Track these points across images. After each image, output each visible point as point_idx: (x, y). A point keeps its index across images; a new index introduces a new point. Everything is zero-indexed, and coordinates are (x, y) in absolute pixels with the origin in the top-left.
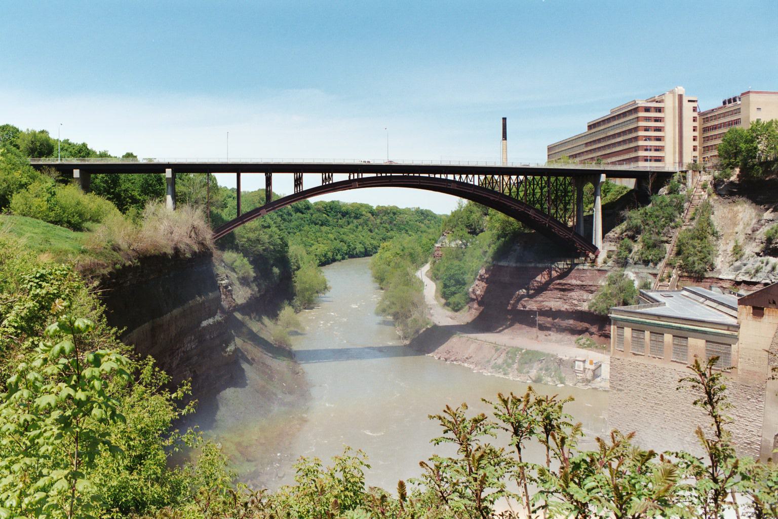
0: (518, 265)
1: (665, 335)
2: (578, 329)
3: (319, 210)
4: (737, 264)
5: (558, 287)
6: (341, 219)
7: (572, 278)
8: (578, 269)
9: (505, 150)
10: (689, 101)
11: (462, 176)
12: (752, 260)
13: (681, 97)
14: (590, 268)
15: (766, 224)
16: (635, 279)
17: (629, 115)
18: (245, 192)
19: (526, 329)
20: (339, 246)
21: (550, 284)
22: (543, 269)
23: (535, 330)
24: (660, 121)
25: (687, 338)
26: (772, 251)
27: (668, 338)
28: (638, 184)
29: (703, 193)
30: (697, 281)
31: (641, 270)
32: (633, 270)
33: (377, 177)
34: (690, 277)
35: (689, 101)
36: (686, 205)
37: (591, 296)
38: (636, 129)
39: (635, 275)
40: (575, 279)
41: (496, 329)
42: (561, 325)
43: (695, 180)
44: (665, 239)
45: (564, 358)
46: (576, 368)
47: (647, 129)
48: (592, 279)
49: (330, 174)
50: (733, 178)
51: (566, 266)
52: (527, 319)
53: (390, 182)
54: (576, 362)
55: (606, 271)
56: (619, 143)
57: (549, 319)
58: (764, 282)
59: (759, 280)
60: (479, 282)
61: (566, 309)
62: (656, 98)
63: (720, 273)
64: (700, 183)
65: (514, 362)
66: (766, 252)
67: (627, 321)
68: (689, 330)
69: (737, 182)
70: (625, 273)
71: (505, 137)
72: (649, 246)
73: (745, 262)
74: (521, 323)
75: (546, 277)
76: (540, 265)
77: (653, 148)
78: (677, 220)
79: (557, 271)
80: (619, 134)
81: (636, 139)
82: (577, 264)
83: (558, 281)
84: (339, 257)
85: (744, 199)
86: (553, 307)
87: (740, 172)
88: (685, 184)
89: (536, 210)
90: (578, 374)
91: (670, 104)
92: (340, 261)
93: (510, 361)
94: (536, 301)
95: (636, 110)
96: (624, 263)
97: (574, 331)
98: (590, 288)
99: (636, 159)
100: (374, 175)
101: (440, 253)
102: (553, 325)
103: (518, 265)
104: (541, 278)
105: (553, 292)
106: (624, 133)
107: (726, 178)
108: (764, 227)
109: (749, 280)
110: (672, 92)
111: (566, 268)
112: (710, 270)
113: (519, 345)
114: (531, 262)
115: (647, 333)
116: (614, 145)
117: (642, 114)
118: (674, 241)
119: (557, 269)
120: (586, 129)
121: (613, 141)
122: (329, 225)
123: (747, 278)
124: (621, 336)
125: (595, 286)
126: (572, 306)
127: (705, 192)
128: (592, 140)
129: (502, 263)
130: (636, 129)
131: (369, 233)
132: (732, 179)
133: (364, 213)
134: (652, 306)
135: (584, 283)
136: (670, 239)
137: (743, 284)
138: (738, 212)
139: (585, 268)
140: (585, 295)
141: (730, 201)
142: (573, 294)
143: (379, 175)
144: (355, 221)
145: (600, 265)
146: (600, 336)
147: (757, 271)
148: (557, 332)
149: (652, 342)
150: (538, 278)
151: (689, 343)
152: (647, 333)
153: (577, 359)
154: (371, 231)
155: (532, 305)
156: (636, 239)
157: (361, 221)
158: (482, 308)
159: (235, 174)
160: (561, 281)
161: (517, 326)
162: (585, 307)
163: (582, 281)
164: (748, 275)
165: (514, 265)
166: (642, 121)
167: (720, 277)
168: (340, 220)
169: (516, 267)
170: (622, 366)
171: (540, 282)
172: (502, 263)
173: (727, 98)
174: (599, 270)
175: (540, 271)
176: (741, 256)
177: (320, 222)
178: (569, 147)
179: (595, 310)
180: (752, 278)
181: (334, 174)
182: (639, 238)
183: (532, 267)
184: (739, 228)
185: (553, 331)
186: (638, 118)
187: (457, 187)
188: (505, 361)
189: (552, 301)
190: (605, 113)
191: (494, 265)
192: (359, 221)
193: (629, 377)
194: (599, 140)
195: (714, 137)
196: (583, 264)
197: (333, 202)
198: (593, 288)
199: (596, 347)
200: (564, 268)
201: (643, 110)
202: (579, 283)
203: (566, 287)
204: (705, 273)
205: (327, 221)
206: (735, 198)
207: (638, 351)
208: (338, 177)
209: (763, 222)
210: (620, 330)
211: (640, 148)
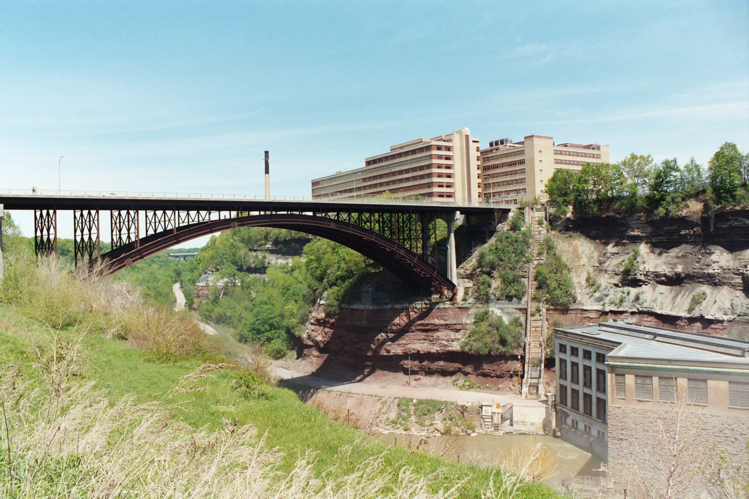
0: (375, 307)
1: (626, 375)
2: (450, 370)
4: (597, 295)
5: (420, 327)
7: (433, 318)
8: (439, 308)
9: (267, 184)
10: (474, 141)
11: (157, 212)
12: (611, 290)
13: (467, 137)
14: (451, 306)
15: (612, 257)
16: (501, 314)
17: (419, 152)
18: (60, 239)
19: (391, 375)
21: (412, 326)
22: (401, 311)
23: (401, 375)
24: (450, 159)
25: (624, 375)
26: (630, 282)
27: (630, 379)
29: (541, 228)
30: (563, 314)
31: (506, 306)
32: (497, 306)
33: (260, 215)
34: (555, 310)
35: (474, 141)
37: (458, 335)
38: (429, 166)
39: (500, 311)
40: (438, 318)
41: (354, 379)
42: (431, 367)
44: (521, 273)
45: (467, 405)
46: (483, 414)
47: (439, 167)
48: (455, 317)
50: (569, 215)
51: (424, 306)
52: (393, 364)
53: (271, 222)
54: (483, 407)
55: (467, 309)
56: (407, 179)
57: (416, 362)
58: (630, 310)
59: (626, 309)
60: (313, 327)
61: (437, 351)
62: (443, 137)
63: (583, 305)
64: (534, 219)
65: (410, 415)
66: (624, 283)
67: (629, 367)
68: (709, 372)
69: (572, 219)
70: (490, 309)
71: (267, 172)
72: (506, 281)
73: (605, 292)
74: (383, 369)
75: (405, 319)
76: (398, 306)
79: (415, 312)
80: (407, 171)
81: (430, 175)
83: (420, 322)
85: (578, 233)
86: (420, 349)
87: (573, 209)
89: (406, 249)
90: (486, 420)
91: (457, 143)
93: (405, 414)
94: (399, 345)
95: (429, 148)
96: (484, 299)
97: (444, 373)
98: (455, 327)
99: (430, 195)
101: (206, 292)
102: (420, 368)
103: (375, 307)
104: (400, 321)
105: (415, 333)
106: (414, 170)
107: (562, 214)
108: (610, 259)
109: (616, 310)
110: (460, 132)
111: (425, 308)
112: (573, 302)
113: (409, 396)
114: (387, 304)
115: (655, 380)
116: (401, 181)
117: (435, 152)
118: (532, 274)
119: (415, 310)
120: (363, 165)
121: (400, 177)
123: (614, 309)
125: (459, 324)
126: (442, 346)
127: (542, 227)
128: (371, 175)
130: (429, 166)
135: (448, 322)
136: (525, 274)
137: (610, 314)
139: (446, 306)
140: (453, 335)
141: (567, 236)
142: (438, 334)
143: (262, 213)
145: (461, 303)
146: (477, 376)
147: (621, 301)
148: (426, 375)
149: (661, 387)
150: (397, 320)
151: (708, 386)
152: (655, 380)
153: (483, 404)
155: (396, 349)
156: (492, 275)
158: (325, 356)
159: (34, 211)
160: (423, 322)
161: (379, 372)
162: (456, 347)
163: (446, 320)
164: (613, 305)
165: (371, 308)
166: (435, 159)
167: (585, 308)
169: (373, 310)
170: (625, 415)
171: (399, 325)
173: (494, 140)
174: (460, 308)
175: (397, 313)
176: (599, 287)
178: (341, 182)
179: (470, 350)
180: (618, 308)
181: (58, 211)
182: (495, 274)
183: (389, 309)
184: (584, 261)
185: (421, 375)
186: (431, 155)
187: (336, 227)
188: (399, 416)
189: (416, 343)
190: (385, 150)
193: (633, 425)
194: (381, 176)
195: (509, 173)
198: (458, 327)
199: (479, 387)
200: (422, 308)
201: (436, 148)
202: (442, 322)
203: (429, 327)
204: (570, 305)
206: (571, 233)
207: (645, 398)
209: (608, 255)
210: (620, 378)
211: (434, 184)
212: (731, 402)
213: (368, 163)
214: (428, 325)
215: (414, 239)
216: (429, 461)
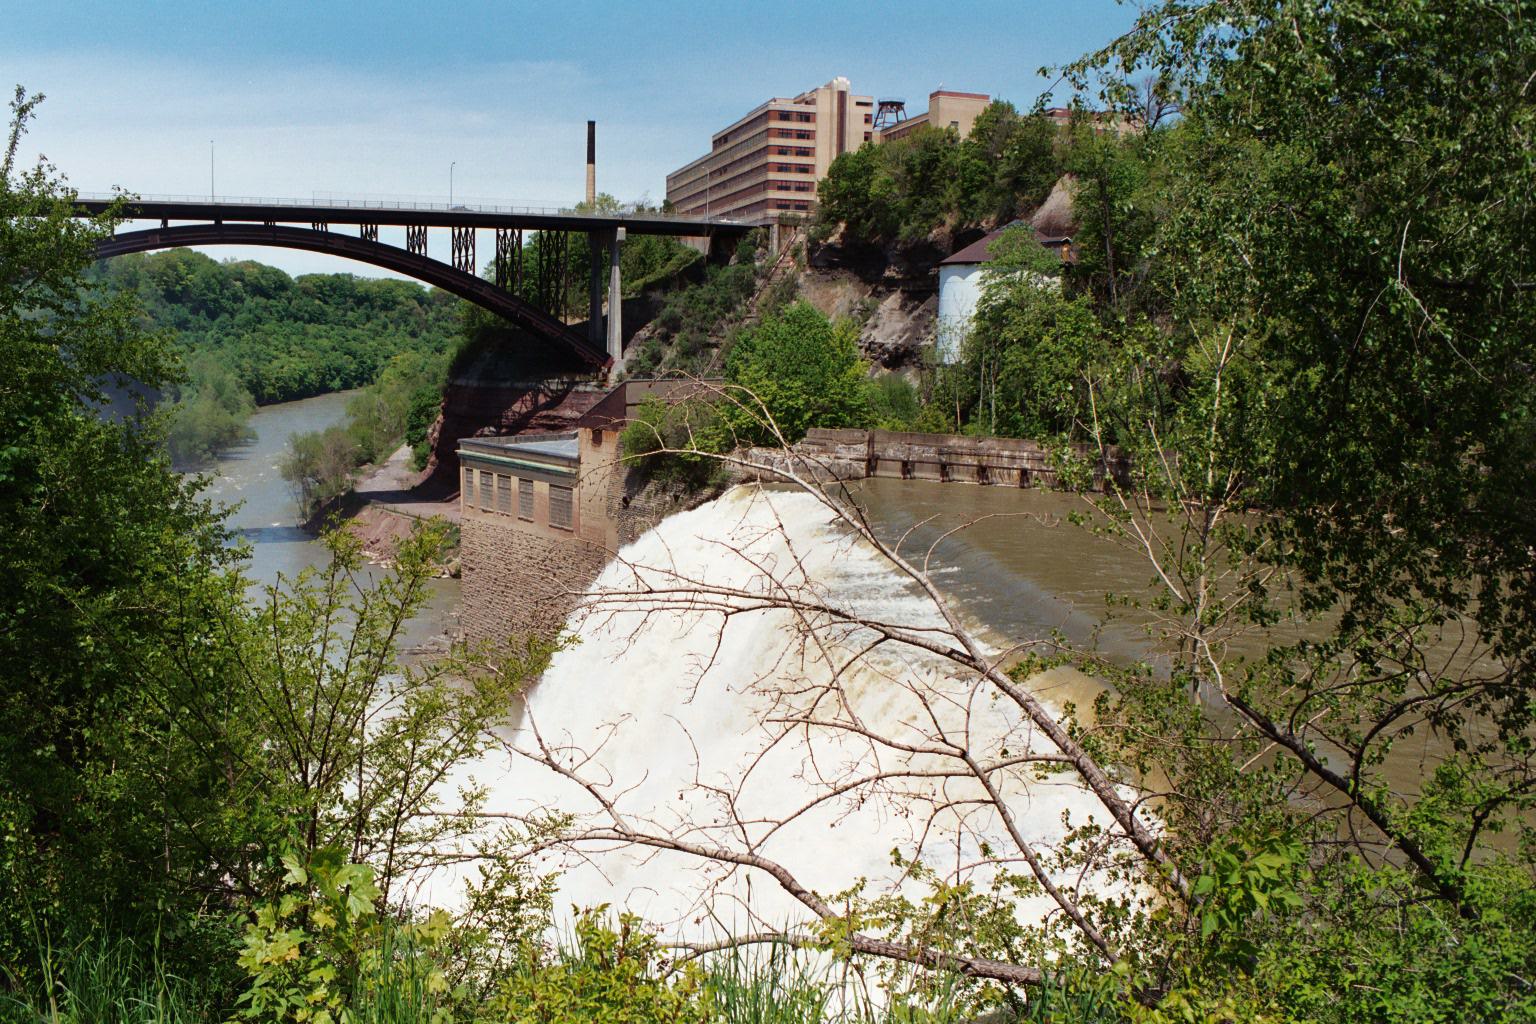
3: (306, 292)
5: (544, 422)
6: (352, 309)
10: (858, 104)
13: (842, 95)
20: (339, 362)
28: (714, 245)
35: (858, 104)
36: (759, 283)
38: (766, 150)
43: (785, 243)
44: (713, 340)
47: (783, 151)
49: (562, 233)
71: (591, 159)
75: (529, 404)
76: (520, 385)
77: (793, 186)
78: (739, 308)
79: (546, 395)
82: (577, 383)
83: (545, 413)
84: (337, 383)
88: (766, 248)
91: (825, 108)
92: (338, 390)
100: (278, 224)
110: (829, 86)
114: (505, 380)
117: (775, 124)
122: (326, 323)
124: (527, 495)
129: (458, 382)
131: (409, 339)
132: (831, 240)
133: (401, 299)
134: (544, 439)
138: (835, 296)
139: (589, 389)
144: (382, 315)
150: (516, 407)
154: (413, 334)
157: (394, 314)
160: (551, 413)
165: (475, 384)
168: (350, 313)
172: (458, 382)
175: (518, 395)
177: (306, 316)
182: (677, 338)
191: (451, 385)
192: (391, 314)
196: (586, 383)
197: (337, 276)
205: (324, 313)
208: (353, 230)
212: (553, 518)
213: (720, 141)
214: (555, 417)
215: (527, 275)
216: (1177, 727)
